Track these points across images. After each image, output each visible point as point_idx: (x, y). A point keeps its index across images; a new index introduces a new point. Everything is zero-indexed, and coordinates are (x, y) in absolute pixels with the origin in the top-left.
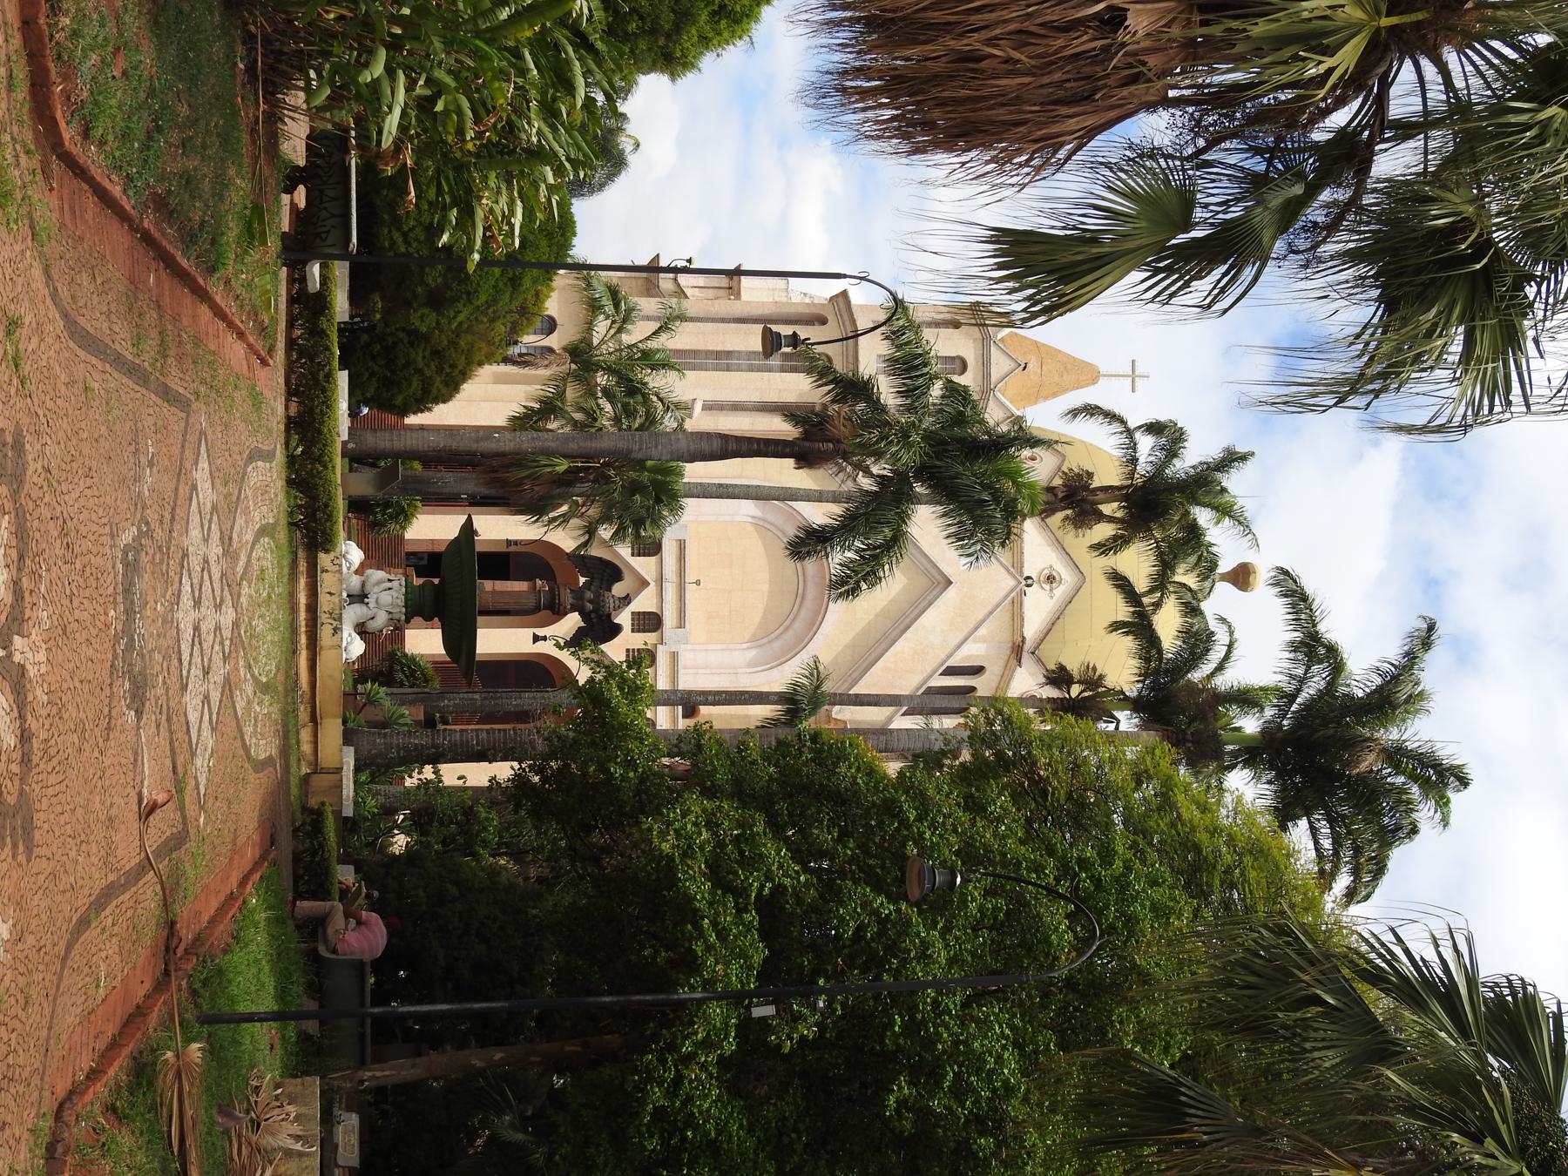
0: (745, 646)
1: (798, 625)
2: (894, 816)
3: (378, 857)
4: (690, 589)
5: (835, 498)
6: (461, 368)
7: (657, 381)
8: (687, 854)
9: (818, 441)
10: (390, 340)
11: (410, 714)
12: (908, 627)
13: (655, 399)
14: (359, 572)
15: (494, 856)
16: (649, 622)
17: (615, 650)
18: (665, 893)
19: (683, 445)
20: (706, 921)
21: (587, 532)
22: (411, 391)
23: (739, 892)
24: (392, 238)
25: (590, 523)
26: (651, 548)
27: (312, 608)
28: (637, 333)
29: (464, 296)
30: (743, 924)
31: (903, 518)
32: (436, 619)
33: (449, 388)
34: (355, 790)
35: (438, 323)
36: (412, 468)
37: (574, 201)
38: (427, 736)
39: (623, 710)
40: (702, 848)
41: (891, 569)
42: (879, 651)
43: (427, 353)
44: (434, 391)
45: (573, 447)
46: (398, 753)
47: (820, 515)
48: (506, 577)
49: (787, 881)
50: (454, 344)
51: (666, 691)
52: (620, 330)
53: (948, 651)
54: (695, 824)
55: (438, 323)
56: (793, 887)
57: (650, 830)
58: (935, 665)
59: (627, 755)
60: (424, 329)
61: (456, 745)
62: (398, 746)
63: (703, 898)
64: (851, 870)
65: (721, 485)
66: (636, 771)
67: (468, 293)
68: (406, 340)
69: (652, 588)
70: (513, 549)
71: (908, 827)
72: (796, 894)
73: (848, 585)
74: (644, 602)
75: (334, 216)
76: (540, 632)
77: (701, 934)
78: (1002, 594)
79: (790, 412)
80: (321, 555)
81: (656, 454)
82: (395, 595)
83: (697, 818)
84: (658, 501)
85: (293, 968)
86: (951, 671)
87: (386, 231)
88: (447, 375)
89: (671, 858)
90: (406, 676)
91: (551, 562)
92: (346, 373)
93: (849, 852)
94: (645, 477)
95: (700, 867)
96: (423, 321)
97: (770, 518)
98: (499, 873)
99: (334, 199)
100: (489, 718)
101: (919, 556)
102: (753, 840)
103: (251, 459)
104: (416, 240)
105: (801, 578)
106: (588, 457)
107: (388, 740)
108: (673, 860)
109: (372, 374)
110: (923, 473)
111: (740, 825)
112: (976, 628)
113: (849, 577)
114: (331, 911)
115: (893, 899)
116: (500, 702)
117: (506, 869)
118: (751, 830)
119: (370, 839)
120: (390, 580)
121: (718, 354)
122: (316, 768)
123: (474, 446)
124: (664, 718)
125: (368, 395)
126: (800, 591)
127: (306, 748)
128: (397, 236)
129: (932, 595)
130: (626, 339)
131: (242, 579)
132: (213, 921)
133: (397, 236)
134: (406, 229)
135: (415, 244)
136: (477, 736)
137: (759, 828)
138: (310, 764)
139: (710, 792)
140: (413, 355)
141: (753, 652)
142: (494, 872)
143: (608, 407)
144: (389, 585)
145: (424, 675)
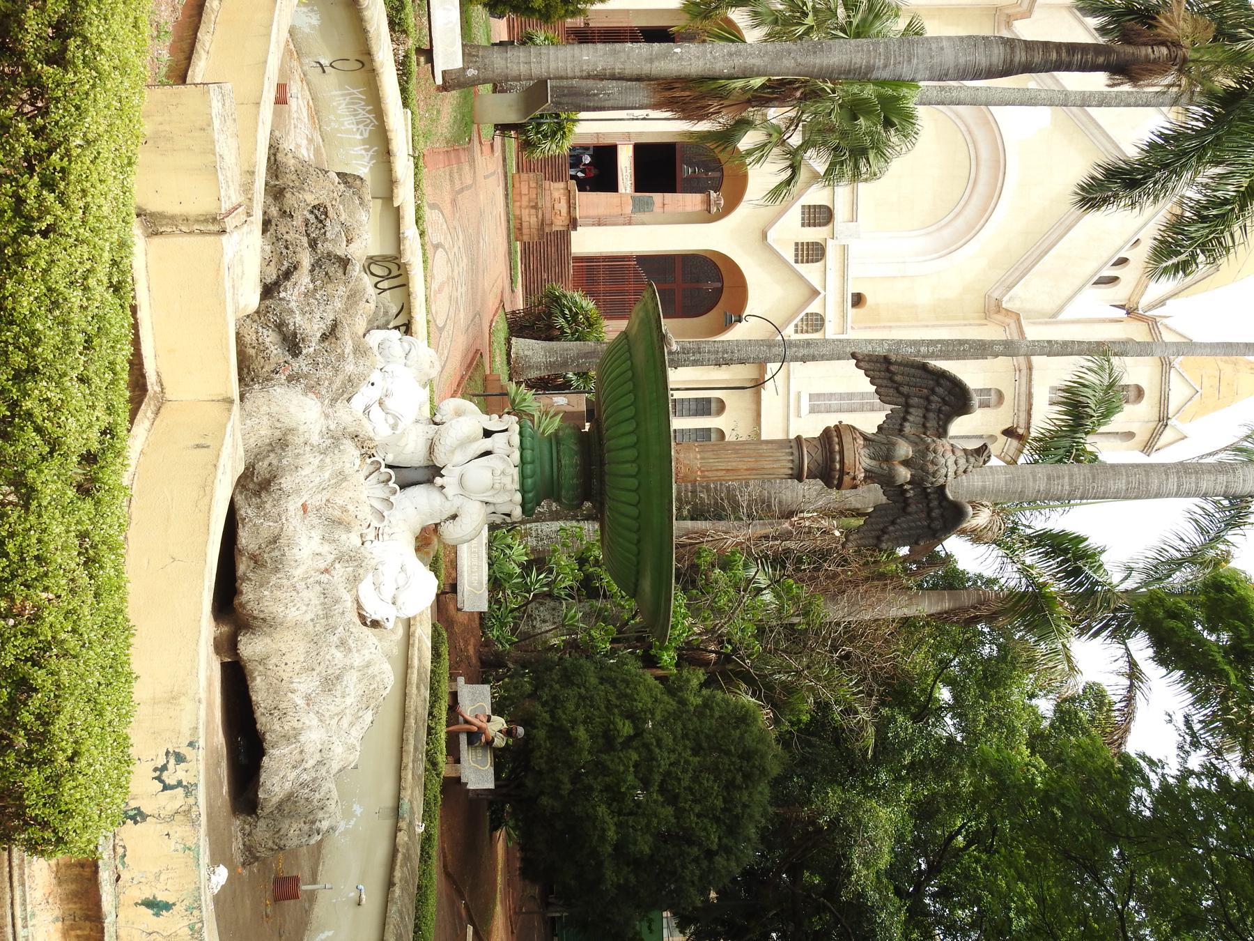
1: (971, 211)
9: (1145, 44)
21: (791, 166)
84: (888, 124)
90: (568, 322)
94: (869, 91)
101: (1101, 138)
105: (973, 163)
126: (973, 175)
144: (487, 444)
145: (587, 319)
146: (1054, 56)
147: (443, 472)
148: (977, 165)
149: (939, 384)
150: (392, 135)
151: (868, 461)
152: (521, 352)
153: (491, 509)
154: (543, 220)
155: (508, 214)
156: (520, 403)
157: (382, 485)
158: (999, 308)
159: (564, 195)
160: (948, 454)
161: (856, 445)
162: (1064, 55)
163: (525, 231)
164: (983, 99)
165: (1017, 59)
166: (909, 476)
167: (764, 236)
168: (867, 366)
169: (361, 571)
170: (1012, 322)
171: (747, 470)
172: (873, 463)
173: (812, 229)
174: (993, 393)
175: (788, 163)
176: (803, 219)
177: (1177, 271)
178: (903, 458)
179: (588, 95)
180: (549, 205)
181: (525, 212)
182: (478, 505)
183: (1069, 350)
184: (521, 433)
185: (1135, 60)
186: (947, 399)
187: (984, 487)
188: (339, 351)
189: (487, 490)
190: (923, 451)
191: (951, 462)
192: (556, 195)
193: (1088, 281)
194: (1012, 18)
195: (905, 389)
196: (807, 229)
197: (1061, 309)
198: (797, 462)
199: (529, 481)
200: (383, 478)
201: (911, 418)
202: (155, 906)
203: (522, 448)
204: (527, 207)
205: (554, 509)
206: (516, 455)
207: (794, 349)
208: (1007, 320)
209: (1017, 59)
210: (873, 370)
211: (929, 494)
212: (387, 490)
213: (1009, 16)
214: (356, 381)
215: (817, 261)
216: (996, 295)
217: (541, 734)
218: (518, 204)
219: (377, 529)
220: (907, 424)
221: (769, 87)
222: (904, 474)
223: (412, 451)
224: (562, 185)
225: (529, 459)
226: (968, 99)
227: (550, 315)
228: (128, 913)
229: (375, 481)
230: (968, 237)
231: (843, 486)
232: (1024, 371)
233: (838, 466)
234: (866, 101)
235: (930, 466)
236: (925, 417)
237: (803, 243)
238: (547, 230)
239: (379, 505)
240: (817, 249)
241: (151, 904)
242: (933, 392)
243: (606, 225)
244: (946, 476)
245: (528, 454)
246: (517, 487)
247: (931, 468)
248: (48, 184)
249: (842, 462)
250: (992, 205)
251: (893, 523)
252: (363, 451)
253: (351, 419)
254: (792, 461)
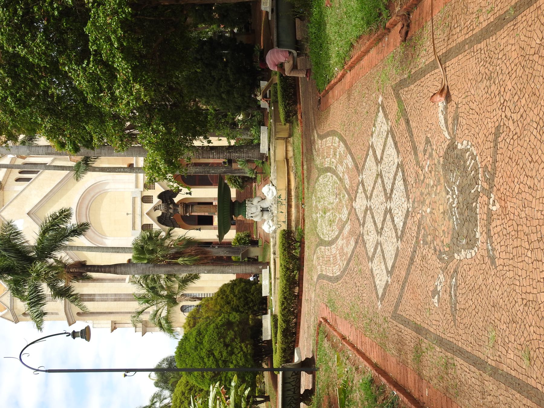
0: (109, 190)
1: (89, 198)
2: (20, 100)
3: (250, 111)
4: (130, 212)
5: (72, 248)
6: (219, 298)
7: (143, 291)
8: (126, 82)
9: (76, 272)
10: (246, 307)
11: (238, 166)
12: (45, 197)
13: (144, 285)
14: (264, 221)
15: (208, 109)
16: (146, 199)
17: (159, 189)
18: (138, 64)
19: (132, 270)
20: (116, 46)
22: (238, 288)
23: (100, 62)
24: (247, 349)
25: (169, 238)
26: (146, 227)
27: (289, 206)
28: (152, 310)
29: (219, 327)
30: (97, 44)
31: (40, 242)
32: (233, 201)
33: (223, 290)
34: (260, 137)
35: (229, 316)
36: (235, 257)
37: (174, 354)
38: (232, 156)
39: (158, 158)
40: (119, 86)
41: (46, 221)
42: (57, 188)
43: (232, 303)
44: (229, 289)
45: (176, 268)
46: (243, 150)
47: (79, 241)
48: (199, 217)
49: (75, 67)
50: (222, 307)
51: (140, 173)
52: (157, 311)
53: (29, 187)
54: (122, 99)
55: (229, 316)
56: (71, 63)
57: (145, 96)
58: (34, 183)
59: (157, 136)
60: (234, 313)
61: (222, 153)
62: (244, 153)
63: (118, 59)
64: (42, 73)
65: (118, 252)
66: (153, 128)
67: (217, 328)
68: (240, 308)
69: (145, 212)
70: (199, 227)
71: (12, 94)
72: (70, 61)
73: (65, 214)
74: (148, 207)
75: (289, 383)
76: (189, 196)
77: (119, 39)
78: (6, 209)
79: (89, 279)
80: (286, 228)
81: (143, 265)
82: (250, 211)
83: (122, 102)
84: (142, 247)
85: (314, 40)
86: (28, 180)
87: (249, 351)
88: (224, 295)
89: (135, 81)
90: (237, 180)
91: (184, 223)
92: (264, 295)
93: (43, 82)
94: (148, 256)
95: (120, 75)
96: (235, 316)
97: (99, 239)
98: (206, 102)
99: (288, 390)
100: (207, 164)
102: (93, 90)
103: (337, 279)
104: (237, 348)
105: (88, 215)
106: (169, 264)
107: (247, 155)
108: (134, 81)
109: (253, 294)
110: (31, 260)
111: (100, 98)
112: (17, 196)
113: (64, 218)
114: (291, 72)
115: (16, 55)
116: (203, 170)
117: (203, 104)
118: (94, 96)
119: (253, 118)
120: (252, 217)
121: (120, 300)
122: (286, 140)
123: (214, 268)
124: (140, 162)
125: (254, 286)
127: (290, 149)
128: (245, 349)
129: (35, 209)
130: (154, 308)
131: (346, 222)
132: (367, 52)
133: (245, 349)
134: (242, 353)
135: (238, 347)
136: (213, 156)
137: (90, 96)
138: (289, 142)
139: (116, 116)
140: (237, 302)
141: (107, 188)
142: (207, 103)
143: (162, 282)
145: (231, 181)
146: (103, 270)
150: (273, 264)
153: (252, 203)
162: (100, 270)
165: (113, 269)
173: (149, 195)
176: (152, 198)
177: (65, 210)
185: (79, 268)
190: (168, 211)
191: (162, 208)
195: (170, 221)
196: (151, 195)
202: (282, 212)
203: (245, 214)
209: (113, 269)
217: (247, 95)
221: (177, 257)
222: (171, 206)
223: (265, 213)
226: (110, 249)
227: (243, 183)
228: (285, 212)
230: (89, 189)
241: (282, 213)
242: (165, 221)
248: (283, 291)
250: (80, 200)
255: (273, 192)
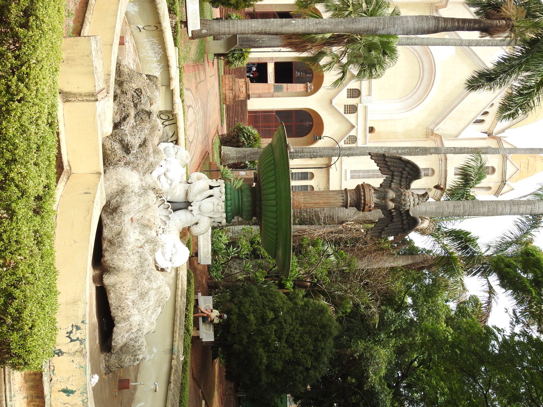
1: (420, 91)
9: (496, 19)
21: (343, 72)
84: (385, 53)
90: (246, 139)
94: (376, 39)
101: (477, 59)
105: (421, 70)
126: (421, 76)
144: (211, 192)
145: (254, 138)
146: (456, 24)
147: (192, 204)
148: (423, 71)
149: (406, 166)
150: (170, 58)
151: (376, 199)
152: (226, 152)
153: (213, 220)
154: (235, 95)
155: (220, 93)
156: (225, 174)
157: (166, 210)
158: (432, 133)
159: (244, 84)
160: (411, 196)
161: (371, 193)
162: (461, 24)
163: (227, 100)
164: (426, 43)
165: (440, 26)
166: (394, 206)
167: (331, 102)
168: (376, 158)
169: (156, 247)
170: (438, 139)
171: (323, 203)
172: (378, 200)
173: (352, 99)
174: (430, 170)
175: (341, 70)
176: (348, 95)
177: (510, 117)
178: (391, 198)
179: (254, 41)
180: (238, 89)
181: (227, 92)
182: (207, 218)
183: (463, 151)
184: (225, 187)
185: (492, 26)
186: (410, 172)
187: (426, 211)
188: (147, 152)
189: (211, 212)
190: (400, 195)
191: (412, 200)
192: (241, 84)
193: (471, 122)
194: (438, 8)
195: (392, 168)
196: (350, 99)
197: (459, 134)
198: (345, 200)
199: (229, 208)
200: (166, 207)
201: (394, 181)
202: (67, 392)
203: (226, 194)
204: (228, 89)
205: (240, 220)
206: (224, 197)
207: (344, 151)
208: (436, 138)
209: (440, 26)
210: (378, 160)
211: (402, 213)
212: (168, 212)
213: (437, 7)
214: (154, 165)
215: (354, 113)
216: (431, 127)
217: (234, 317)
218: (224, 88)
219: (163, 229)
220: (393, 184)
221: (333, 38)
222: (391, 205)
224: (243, 80)
225: (229, 199)
226: (419, 43)
227: (238, 136)
228: (55, 395)
229: (162, 208)
230: (419, 103)
231: (365, 210)
232: (444, 161)
233: (363, 202)
234: (375, 44)
235: (403, 202)
236: (400, 180)
237: (348, 105)
238: (237, 99)
239: (164, 219)
240: (354, 108)
241: (65, 391)
242: (404, 169)
243: (262, 97)
244: (410, 206)
245: (229, 196)
246: (224, 211)
247: (403, 203)
248: (21, 79)
249: (365, 200)
250: (430, 89)
251: (387, 226)
252: (157, 195)
253: (152, 181)
254: (343, 199)
255: (163, 254)
